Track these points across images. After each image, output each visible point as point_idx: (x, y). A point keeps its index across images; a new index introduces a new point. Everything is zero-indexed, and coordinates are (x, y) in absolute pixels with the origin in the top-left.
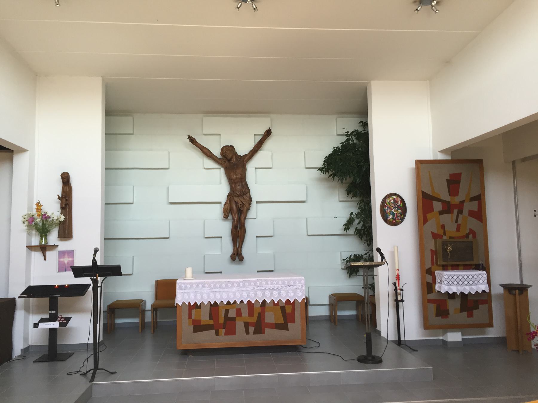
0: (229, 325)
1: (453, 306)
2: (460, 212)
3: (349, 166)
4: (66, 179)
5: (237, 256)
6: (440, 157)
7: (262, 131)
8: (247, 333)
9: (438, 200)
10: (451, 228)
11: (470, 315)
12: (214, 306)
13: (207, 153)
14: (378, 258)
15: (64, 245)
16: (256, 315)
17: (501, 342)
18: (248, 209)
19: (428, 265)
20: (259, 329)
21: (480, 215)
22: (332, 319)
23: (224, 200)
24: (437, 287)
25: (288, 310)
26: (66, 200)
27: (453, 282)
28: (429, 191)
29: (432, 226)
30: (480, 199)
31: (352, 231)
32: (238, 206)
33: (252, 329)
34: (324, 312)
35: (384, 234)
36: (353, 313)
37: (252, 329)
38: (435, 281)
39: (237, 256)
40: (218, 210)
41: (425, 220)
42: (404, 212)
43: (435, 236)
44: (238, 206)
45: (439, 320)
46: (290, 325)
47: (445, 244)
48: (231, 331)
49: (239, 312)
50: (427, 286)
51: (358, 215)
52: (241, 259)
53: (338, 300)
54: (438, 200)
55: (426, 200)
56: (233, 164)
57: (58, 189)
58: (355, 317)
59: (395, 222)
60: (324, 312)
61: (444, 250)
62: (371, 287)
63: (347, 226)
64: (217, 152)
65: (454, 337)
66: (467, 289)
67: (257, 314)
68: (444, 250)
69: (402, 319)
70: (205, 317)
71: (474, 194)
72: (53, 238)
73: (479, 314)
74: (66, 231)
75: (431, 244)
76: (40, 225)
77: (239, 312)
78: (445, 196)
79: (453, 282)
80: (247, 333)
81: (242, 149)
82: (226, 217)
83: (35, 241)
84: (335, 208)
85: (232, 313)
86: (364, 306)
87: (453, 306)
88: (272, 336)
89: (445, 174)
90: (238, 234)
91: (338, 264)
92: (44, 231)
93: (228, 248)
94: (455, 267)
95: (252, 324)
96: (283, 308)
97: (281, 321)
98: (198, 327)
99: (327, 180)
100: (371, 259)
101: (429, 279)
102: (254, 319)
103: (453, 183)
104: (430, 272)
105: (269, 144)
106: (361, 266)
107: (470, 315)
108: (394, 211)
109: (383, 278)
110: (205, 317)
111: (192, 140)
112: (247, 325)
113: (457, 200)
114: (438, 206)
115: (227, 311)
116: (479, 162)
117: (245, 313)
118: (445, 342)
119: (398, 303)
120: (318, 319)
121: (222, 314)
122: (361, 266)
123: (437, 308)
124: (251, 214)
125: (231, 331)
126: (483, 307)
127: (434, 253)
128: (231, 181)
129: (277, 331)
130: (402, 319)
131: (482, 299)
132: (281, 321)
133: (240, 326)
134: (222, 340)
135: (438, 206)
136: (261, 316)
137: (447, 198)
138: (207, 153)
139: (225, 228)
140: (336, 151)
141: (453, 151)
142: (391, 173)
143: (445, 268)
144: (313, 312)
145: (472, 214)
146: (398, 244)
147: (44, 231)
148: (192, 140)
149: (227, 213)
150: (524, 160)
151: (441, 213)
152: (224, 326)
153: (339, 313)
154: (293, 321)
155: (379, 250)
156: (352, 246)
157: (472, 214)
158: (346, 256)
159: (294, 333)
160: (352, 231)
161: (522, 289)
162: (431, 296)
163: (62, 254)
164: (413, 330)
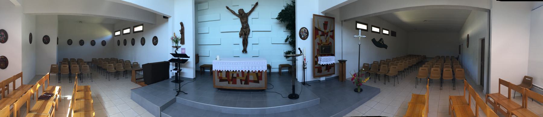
0: (234, 80)
1: (323, 69)
2: (327, 36)
3: (288, 17)
4: (182, 24)
5: (245, 51)
6: (321, 14)
7: (255, 4)
8: (242, 84)
9: (320, 31)
10: (324, 41)
11: (328, 71)
12: (228, 72)
13: (234, 13)
14: (298, 52)
15: (182, 46)
16: (245, 76)
17: (337, 78)
18: (249, 34)
19: (316, 54)
20: (247, 83)
21: (333, 37)
22: (280, 73)
23: (239, 30)
24: (319, 63)
25: (259, 75)
26: (182, 32)
27: (324, 60)
28: (317, 27)
29: (318, 40)
30: (333, 31)
31: (288, 42)
32: (245, 33)
33: (243, 82)
34: (277, 70)
35: (300, 43)
36: (287, 70)
37: (243, 82)
38: (318, 60)
39: (245, 51)
40: (238, 34)
41: (316, 38)
42: (308, 35)
43: (319, 44)
44: (245, 33)
45: (319, 74)
46: (260, 81)
47: (322, 47)
48: (235, 83)
49: (238, 75)
50: (315, 62)
51: (290, 37)
52: (246, 52)
53: (282, 67)
54: (320, 31)
55: (316, 30)
56: (243, 16)
57: (180, 28)
58: (289, 71)
59: (304, 39)
60: (277, 70)
61: (322, 49)
62: (294, 61)
63: (286, 40)
64: (237, 12)
65: (323, 79)
66: (329, 63)
67: (246, 76)
68: (322, 49)
69: (304, 73)
70: (224, 76)
71: (331, 30)
72: (179, 44)
73: (331, 71)
74: (183, 42)
75: (317, 47)
76: (175, 40)
77: (238, 75)
78: (322, 29)
79: (324, 60)
80: (242, 84)
81: (246, 11)
82: (240, 37)
83: (175, 45)
84: (282, 34)
85: (235, 75)
86: (292, 69)
87: (323, 69)
88: (252, 85)
89: (323, 21)
90: (245, 43)
91: (283, 54)
92: (177, 42)
93: (241, 48)
94: (325, 55)
95: (243, 80)
96: (257, 74)
97: (256, 79)
98: (221, 80)
99: (279, 23)
100: (295, 52)
101: (316, 59)
102: (244, 78)
103: (325, 24)
104: (317, 57)
105: (257, 9)
106: (291, 54)
107: (328, 71)
108: (304, 35)
109: (299, 61)
110: (224, 76)
111: (228, 8)
112: (241, 80)
113: (327, 31)
114: (320, 33)
115: (233, 74)
116: (334, 18)
117: (240, 75)
118: (320, 81)
119: (304, 68)
120: (274, 73)
121: (231, 75)
122: (291, 54)
123: (318, 69)
124: (250, 36)
125: (235, 83)
126: (332, 68)
127: (318, 50)
128: (242, 23)
129: (255, 84)
130: (304, 73)
131: (333, 65)
132: (256, 79)
133: (238, 81)
134: (231, 86)
135: (320, 33)
136: (247, 77)
137: (323, 30)
138: (234, 13)
139: (241, 40)
140: (283, 11)
141: (325, 12)
142: (304, 20)
143: (321, 56)
144: (273, 70)
145: (331, 36)
146: (305, 46)
147: (177, 42)
148: (228, 8)
149: (241, 35)
150: (345, 21)
151: (321, 35)
152: (232, 80)
153: (282, 71)
154: (261, 79)
155: (299, 49)
156: (288, 48)
157: (331, 36)
158: (285, 51)
159: (262, 84)
160: (288, 42)
161: (345, 61)
162: (317, 66)
163: (182, 49)
164: (309, 77)
